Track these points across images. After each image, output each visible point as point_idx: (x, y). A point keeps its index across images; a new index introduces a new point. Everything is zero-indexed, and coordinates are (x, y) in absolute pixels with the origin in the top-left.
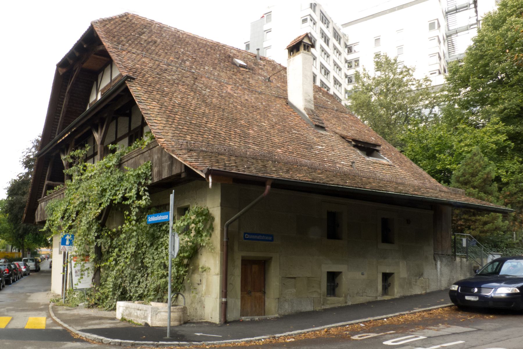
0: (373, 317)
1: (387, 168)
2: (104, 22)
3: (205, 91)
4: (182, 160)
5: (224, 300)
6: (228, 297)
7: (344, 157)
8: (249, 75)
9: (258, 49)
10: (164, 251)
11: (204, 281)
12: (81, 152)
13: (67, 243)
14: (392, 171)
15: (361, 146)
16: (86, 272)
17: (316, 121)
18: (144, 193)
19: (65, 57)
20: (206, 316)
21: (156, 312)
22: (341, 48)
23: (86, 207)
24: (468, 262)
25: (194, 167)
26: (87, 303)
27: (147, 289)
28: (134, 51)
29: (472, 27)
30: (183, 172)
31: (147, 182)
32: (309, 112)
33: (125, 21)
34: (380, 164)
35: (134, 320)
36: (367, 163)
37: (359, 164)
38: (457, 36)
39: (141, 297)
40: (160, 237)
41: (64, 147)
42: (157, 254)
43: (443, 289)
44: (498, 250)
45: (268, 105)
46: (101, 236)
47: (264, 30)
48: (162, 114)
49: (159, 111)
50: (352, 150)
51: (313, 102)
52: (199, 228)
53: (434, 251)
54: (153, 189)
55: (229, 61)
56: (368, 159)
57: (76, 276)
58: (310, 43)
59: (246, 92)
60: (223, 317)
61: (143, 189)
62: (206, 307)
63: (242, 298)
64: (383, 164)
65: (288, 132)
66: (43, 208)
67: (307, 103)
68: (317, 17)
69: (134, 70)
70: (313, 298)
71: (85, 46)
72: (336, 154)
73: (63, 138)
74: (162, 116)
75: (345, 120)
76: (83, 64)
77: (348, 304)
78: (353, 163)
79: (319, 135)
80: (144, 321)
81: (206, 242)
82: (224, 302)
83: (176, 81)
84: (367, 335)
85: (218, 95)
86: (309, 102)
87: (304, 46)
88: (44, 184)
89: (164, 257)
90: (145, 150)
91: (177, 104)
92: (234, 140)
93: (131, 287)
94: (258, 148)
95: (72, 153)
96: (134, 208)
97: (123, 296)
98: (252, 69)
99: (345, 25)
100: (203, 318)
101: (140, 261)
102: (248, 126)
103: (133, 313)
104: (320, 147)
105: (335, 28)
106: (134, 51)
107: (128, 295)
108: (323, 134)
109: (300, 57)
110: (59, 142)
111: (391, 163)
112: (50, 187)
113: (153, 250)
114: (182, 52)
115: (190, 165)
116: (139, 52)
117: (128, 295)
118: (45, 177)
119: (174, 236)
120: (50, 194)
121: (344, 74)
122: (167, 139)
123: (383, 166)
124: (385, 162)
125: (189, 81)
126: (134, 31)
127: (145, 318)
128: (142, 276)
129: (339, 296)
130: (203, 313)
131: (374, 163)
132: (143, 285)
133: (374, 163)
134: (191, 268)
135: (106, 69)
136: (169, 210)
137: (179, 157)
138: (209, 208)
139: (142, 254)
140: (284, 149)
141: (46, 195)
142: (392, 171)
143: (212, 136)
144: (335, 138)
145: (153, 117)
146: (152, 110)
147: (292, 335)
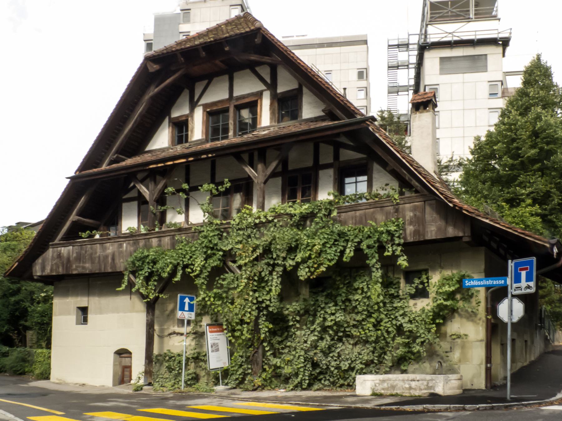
5: (489, 365)
13: (187, 308)
38: (398, 95)
47: (181, 31)
110: (151, 166)
121: (468, 148)
136: (506, 275)
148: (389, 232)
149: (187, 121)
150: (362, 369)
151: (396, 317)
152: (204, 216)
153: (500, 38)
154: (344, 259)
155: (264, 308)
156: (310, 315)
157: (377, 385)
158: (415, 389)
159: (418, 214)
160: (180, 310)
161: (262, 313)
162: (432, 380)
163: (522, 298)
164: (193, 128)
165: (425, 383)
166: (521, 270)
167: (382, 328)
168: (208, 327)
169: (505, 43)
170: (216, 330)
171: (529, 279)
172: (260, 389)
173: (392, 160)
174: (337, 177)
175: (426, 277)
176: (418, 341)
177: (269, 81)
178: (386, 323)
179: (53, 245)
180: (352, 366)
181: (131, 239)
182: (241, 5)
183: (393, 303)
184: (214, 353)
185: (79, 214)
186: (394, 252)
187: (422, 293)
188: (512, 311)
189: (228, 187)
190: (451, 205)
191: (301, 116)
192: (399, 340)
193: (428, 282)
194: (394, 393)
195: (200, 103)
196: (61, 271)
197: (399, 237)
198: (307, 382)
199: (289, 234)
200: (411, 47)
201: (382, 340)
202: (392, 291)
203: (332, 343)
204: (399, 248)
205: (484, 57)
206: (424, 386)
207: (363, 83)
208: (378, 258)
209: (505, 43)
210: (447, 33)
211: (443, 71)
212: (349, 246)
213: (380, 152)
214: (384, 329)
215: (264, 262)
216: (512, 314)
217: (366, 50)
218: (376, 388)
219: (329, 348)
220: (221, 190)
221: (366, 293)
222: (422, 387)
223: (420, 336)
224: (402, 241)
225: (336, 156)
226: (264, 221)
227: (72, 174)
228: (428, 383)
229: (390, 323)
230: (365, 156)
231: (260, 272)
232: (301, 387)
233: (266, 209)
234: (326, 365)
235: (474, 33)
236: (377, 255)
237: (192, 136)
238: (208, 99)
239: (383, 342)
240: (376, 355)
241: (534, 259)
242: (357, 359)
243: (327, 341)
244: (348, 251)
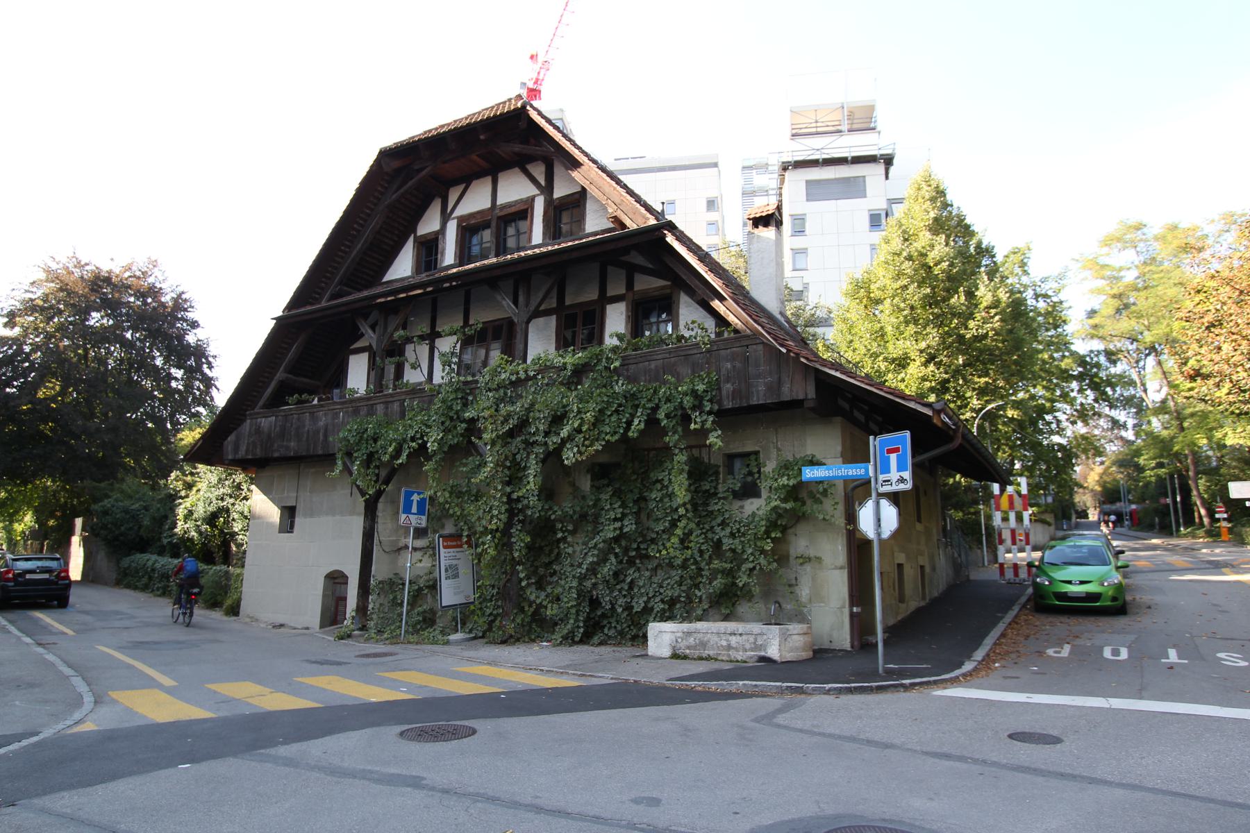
13: (414, 509)
109: (768, 233)
110: (379, 301)
148: (694, 393)
149: (436, 240)
150: (663, 610)
151: (712, 527)
152: (443, 370)
153: (881, 155)
154: (630, 434)
155: (520, 511)
156: (588, 522)
157: (680, 640)
158: (736, 649)
159: (738, 365)
161: (516, 519)
162: (762, 634)
163: (895, 498)
164: (444, 249)
165: (752, 639)
166: (890, 451)
167: (692, 545)
168: (441, 539)
169: (888, 161)
170: (454, 543)
171: (901, 468)
172: (512, 640)
173: (701, 286)
174: (630, 314)
175: (756, 463)
176: (745, 567)
177: (543, 183)
178: (697, 536)
179: (251, 415)
180: (650, 606)
181: (350, 405)
183: (708, 505)
184: (449, 581)
185: (286, 371)
186: (703, 422)
187: (750, 491)
188: (879, 520)
189: (479, 329)
190: (784, 350)
191: (584, 229)
192: (716, 564)
193: (759, 472)
194: (704, 656)
195: (455, 215)
196: (259, 453)
197: (711, 401)
198: (582, 630)
199: (554, 397)
200: (770, 168)
201: (692, 564)
202: (706, 486)
203: (620, 567)
204: (711, 418)
205: (861, 179)
206: (750, 644)
207: (713, 216)
208: (681, 433)
209: (888, 161)
211: (810, 197)
212: (639, 414)
213: (684, 276)
214: (695, 546)
215: (519, 439)
216: (880, 526)
217: (717, 174)
218: (678, 646)
219: (616, 574)
220: (469, 333)
221: (667, 487)
222: (748, 646)
223: (747, 559)
224: (716, 407)
225: (630, 286)
226: (523, 377)
227: (280, 313)
228: (756, 639)
229: (703, 536)
230: (669, 283)
231: (514, 455)
232: (573, 640)
233: (529, 361)
234: (611, 603)
235: (847, 150)
236: (680, 429)
237: (442, 261)
238: (464, 209)
239: (693, 567)
240: (684, 588)
241: (908, 434)
242: (657, 594)
243: (612, 564)
244: (636, 421)
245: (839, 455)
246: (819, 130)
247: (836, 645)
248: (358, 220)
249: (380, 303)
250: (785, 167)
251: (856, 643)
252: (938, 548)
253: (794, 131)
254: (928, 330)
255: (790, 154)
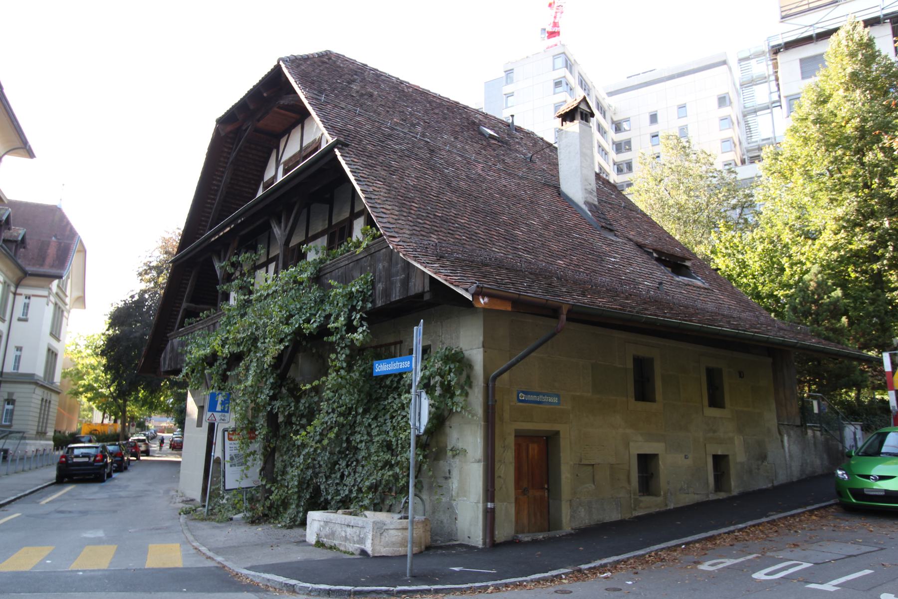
0: (717, 530)
1: (705, 294)
2: (296, 62)
3: (447, 169)
4: (432, 272)
5: (489, 505)
6: (496, 501)
7: (647, 275)
8: (502, 151)
9: (512, 116)
10: (389, 421)
11: (455, 474)
12: (251, 256)
14: (711, 297)
15: (665, 260)
16: (251, 459)
17: (602, 220)
18: (361, 322)
19: (231, 109)
20: (459, 534)
21: (380, 529)
22: (607, 125)
23: (256, 347)
24: (823, 437)
25: (452, 284)
26: (248, 514)
27: (356, 488)
28: (343, 105)
29: (774, 105)
30: (428, 291)
31: (364, 305)
32: (592, 208)
33: (326, 63)
34: (694, 287)
35: (340, 544)
36: (677, 285)
37: (667, 286)
38: (757, 116)
39: (345, 504)
40: (381, 397)
41: (220, 247)
42: (377, 426)
43: (795, 480)
44: (856, 419)
45: (534, 194)
46: (278, 396)
48: (392, 200)
49: (386, 195)
50: (654, 265)
51: (595, 194)
52: (449, 381)
53: (779, 420)
54: (374, 317)
55: (474, 130)
56: (677, 279)
57: (231, 466)
58: (589, 110)
59: (503, 175)
60: (488, 536)
61: (358, 316)
62: (459, 518)
63: (517, 501)
64: (698, 288)
65: (567, 235)
66: (175, 347)
67: (588, 195)
68: (574, 82)
69: (346, 133)
70: (620, 498)
71: (265, 95)
72: (635, 270)
73: (221, 234)
74: (392, 203)
75: (638, 222)
76: (258, 121)
77: (669, 508)
78: (660, 284)
79: (608, 242)
80: (358, 546)
81: (461, 405)
82: (491, 508)
83: (406, 152)
84: (722, 563)
85: (467, 176)
86: (590, 193)
87: (582, 113)
88: (180, 308)
89: (388, 432)
90: (362, 256)
91: (412, 186)
92: (497, 244)
93: (329, 485)
94: (532, 257)
95: (234, 259)
96: (342, 348)
97: (313, 500)
98: (506, 143)
99: (610, 94)
100: (453, 538)
101: (345, 438)
102: (513, 223)
103: (337, 533)
104: (613, 260)
105: (598, 97)
106: (343, 105)
107: (322, 499)
108: (613, 241)
109: (574, 127)
110: (213, 239)
111: (707, 285)
112: (192, 314)
113: (370, 420)
114: (410, 112)
115: (446, 280)
116: (349, 107)
117: (322, 499)
118: (183, 296)
119: (420, 396)
120: (189, 324)
121: (612, 161)
122: (403, 239)
123: (698, 289)
124: (699, 283)
125: (424, 154)
126: (340, 77)
127: (362, 540)
128: (347, 466)
129: (657, 494)
130: (455, 530)
131: (686, 285)
132: (349, 481)
133: (686, 285)
134: (434, 450)
135: (293, 131)
137: (425, 267)
138: (463, 349)
139: (348, 427)
140: (567, 260)
141: (183, 327)
142: (711, 297)
143: (466, 237)
144: (629, 247)
145: (379, 204)
146: (376, 193)
147: (605, 565)
153: (885, 15)
160: (209, 411)
182: (564, 53)
184: (234, 468)
210: (806, 26)
245: (481, 345)
246: (811, 6)
247: (462, 539)
248: (214, 177)
249: (215, 240)
250: (776, 50)
251: (488, 540)
252: (780, 433)
253: (784, 14)
254: (844, 195)
255: (780, 37)
